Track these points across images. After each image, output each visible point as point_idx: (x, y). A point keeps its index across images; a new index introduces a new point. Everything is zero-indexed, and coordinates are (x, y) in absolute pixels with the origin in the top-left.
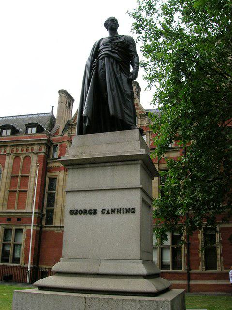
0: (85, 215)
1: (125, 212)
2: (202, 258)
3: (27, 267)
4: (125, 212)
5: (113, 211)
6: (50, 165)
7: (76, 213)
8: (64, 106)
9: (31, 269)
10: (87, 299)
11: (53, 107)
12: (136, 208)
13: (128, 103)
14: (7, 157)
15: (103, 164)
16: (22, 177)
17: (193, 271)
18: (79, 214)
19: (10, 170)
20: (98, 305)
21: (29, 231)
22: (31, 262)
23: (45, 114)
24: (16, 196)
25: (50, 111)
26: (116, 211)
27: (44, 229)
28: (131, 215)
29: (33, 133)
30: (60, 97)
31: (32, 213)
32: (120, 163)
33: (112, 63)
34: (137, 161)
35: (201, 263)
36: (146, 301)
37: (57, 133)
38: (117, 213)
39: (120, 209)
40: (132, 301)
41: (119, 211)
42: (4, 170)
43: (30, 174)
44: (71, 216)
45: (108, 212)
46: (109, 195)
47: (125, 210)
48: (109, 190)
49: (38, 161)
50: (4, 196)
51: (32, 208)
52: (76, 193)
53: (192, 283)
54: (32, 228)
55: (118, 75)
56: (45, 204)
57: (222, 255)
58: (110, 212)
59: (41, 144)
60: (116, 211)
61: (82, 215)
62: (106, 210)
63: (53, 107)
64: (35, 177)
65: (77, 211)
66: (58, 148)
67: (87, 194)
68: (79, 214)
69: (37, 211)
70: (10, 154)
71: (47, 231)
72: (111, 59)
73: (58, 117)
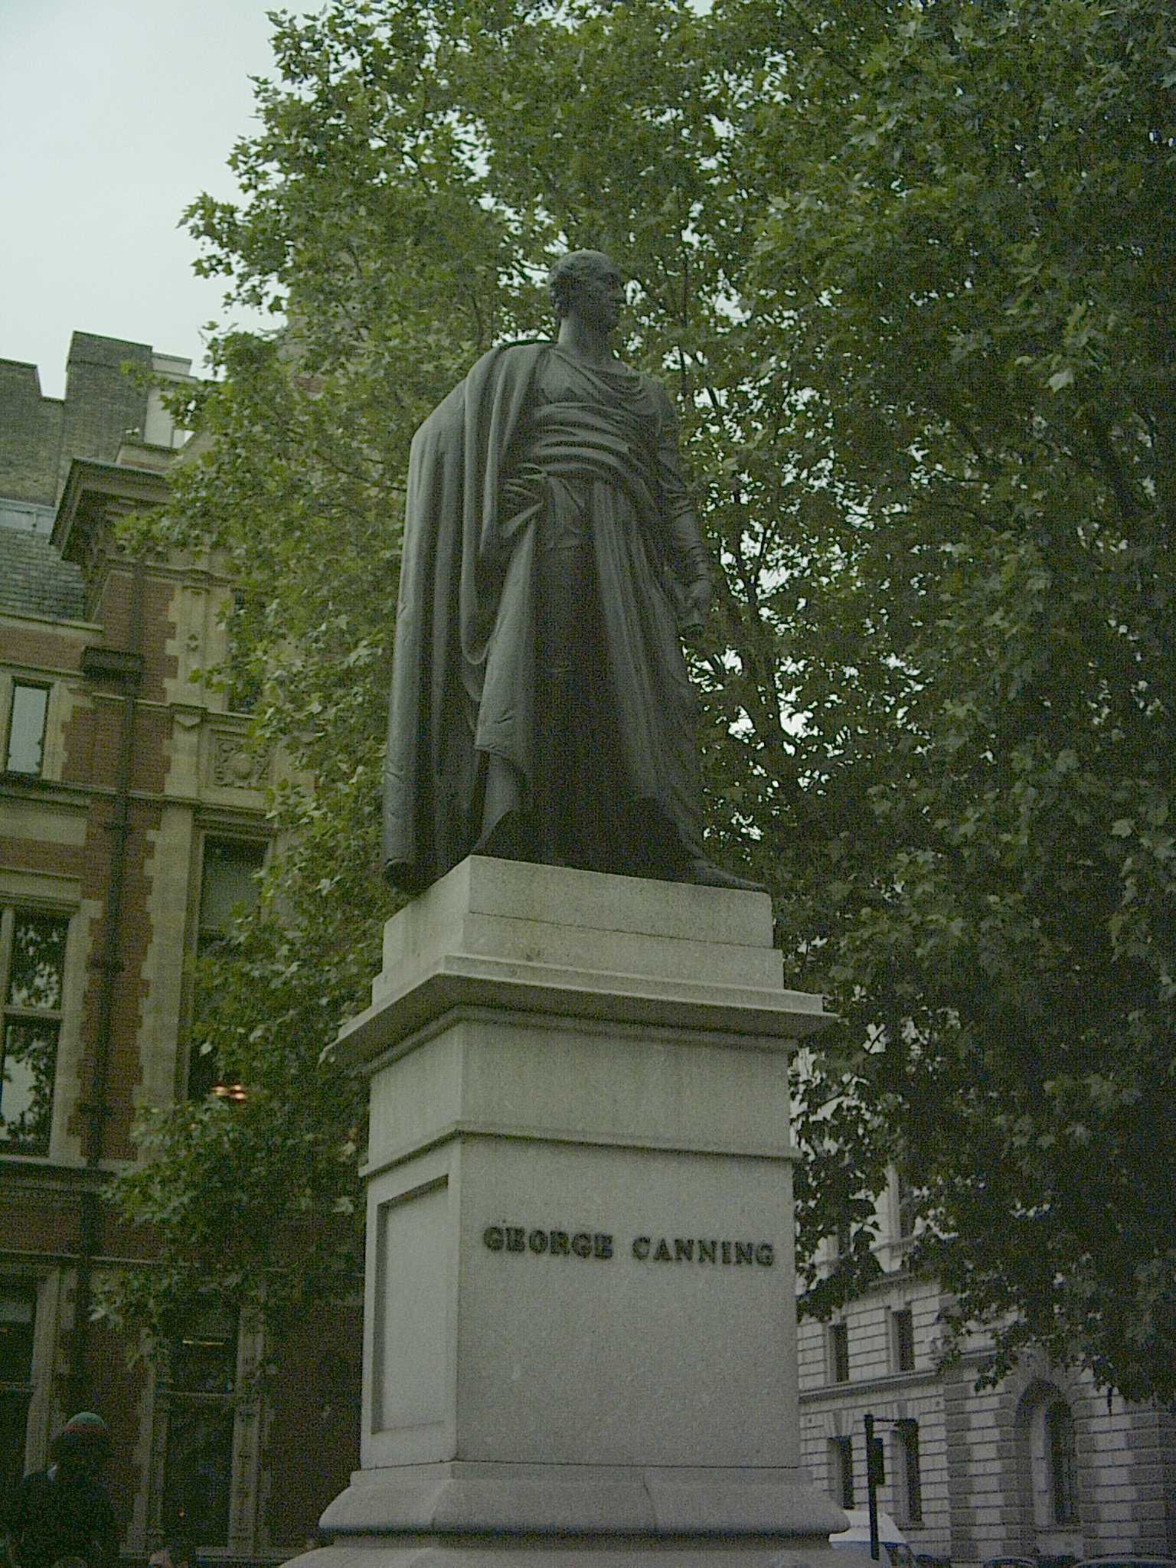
0: (558, 1261)
2: (153, 1472)
5: (684, 1249)
7: (516, 1247)
15: (637, 1030)
26: (622, 1247)
32: (708, 1037)
34: (781, 1042)
38: (701, 1260)
39: (714, 1243)
44: (494, 1258)
45: (662, 1254)
46: (663, 1175)
48: (666, 1151)
52: (509, 1150)
57: (269, 1458)
58: (672, 1252)
60: (696, 1249)
61: (545, 1257)
67: (565, 1159)
68: (528, 1253)
72: (621, 497)
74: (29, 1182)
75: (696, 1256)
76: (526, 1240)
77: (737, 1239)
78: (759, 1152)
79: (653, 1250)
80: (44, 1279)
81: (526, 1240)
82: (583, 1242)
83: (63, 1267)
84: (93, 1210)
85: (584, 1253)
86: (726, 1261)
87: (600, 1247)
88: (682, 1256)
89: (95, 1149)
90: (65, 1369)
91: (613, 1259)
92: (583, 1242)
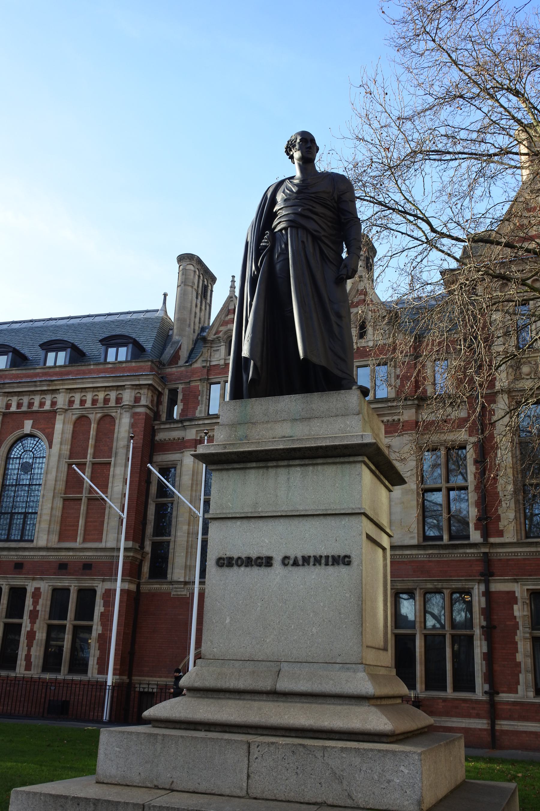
1: (330, 563)
3: (106, 682)
4: (330, 563)
5: (306, 560)
6: (161, 436)
8: (192, 295)
9: (114, 686)
10: (252, 747)
11: (165, 295)
12: (353, 556)
14: (58, 417)
16: (94, 464)
17: (504, 697)
18: (235, 568)
19: (66, 449)
21: (109, 595)
22: (115, 669)
24: (79, 509)
25: (158, 306)
27: (145, 588)
28: (343, 570)
29: (119, 359)
30: (184, 274)
31: (119, 549)
33: (303, 242)
35: (522, 677)
36: (372, 750)
37: (175, 358)
39: (321, 557)
41: (317, 560)
42: (50, 447)
43: (113, 459)
45: (295, 563)
47: (330, 559)
49: (133, 425)
50: (52, 508)
51: (118, 540)
53: (504, 725)
54: (119, 585)
56: (150, 529)
58: (300, 562)
59: (140, 386)
60: (312, 560)
61: (243, 569)
62: (292, 557)
63: (165, 295)
64: (126, 466)
66: (180, 397)
69: (130, 544)
71: (153, 595)
73: (180, 319)
74: (461, 551)
75: (312, 563)
76: (234, 562)
77: (333, 554)
79: (291, 562)
80: (473, 588)
82: (259, 561)
83: (478, 583)
84: (487, 559)
85: (260, 565)
86: (327, 564)
87: (267, 562)
88: (306, 564)
89: (486, 535)
90: (484, 623)
92: (259, 561)
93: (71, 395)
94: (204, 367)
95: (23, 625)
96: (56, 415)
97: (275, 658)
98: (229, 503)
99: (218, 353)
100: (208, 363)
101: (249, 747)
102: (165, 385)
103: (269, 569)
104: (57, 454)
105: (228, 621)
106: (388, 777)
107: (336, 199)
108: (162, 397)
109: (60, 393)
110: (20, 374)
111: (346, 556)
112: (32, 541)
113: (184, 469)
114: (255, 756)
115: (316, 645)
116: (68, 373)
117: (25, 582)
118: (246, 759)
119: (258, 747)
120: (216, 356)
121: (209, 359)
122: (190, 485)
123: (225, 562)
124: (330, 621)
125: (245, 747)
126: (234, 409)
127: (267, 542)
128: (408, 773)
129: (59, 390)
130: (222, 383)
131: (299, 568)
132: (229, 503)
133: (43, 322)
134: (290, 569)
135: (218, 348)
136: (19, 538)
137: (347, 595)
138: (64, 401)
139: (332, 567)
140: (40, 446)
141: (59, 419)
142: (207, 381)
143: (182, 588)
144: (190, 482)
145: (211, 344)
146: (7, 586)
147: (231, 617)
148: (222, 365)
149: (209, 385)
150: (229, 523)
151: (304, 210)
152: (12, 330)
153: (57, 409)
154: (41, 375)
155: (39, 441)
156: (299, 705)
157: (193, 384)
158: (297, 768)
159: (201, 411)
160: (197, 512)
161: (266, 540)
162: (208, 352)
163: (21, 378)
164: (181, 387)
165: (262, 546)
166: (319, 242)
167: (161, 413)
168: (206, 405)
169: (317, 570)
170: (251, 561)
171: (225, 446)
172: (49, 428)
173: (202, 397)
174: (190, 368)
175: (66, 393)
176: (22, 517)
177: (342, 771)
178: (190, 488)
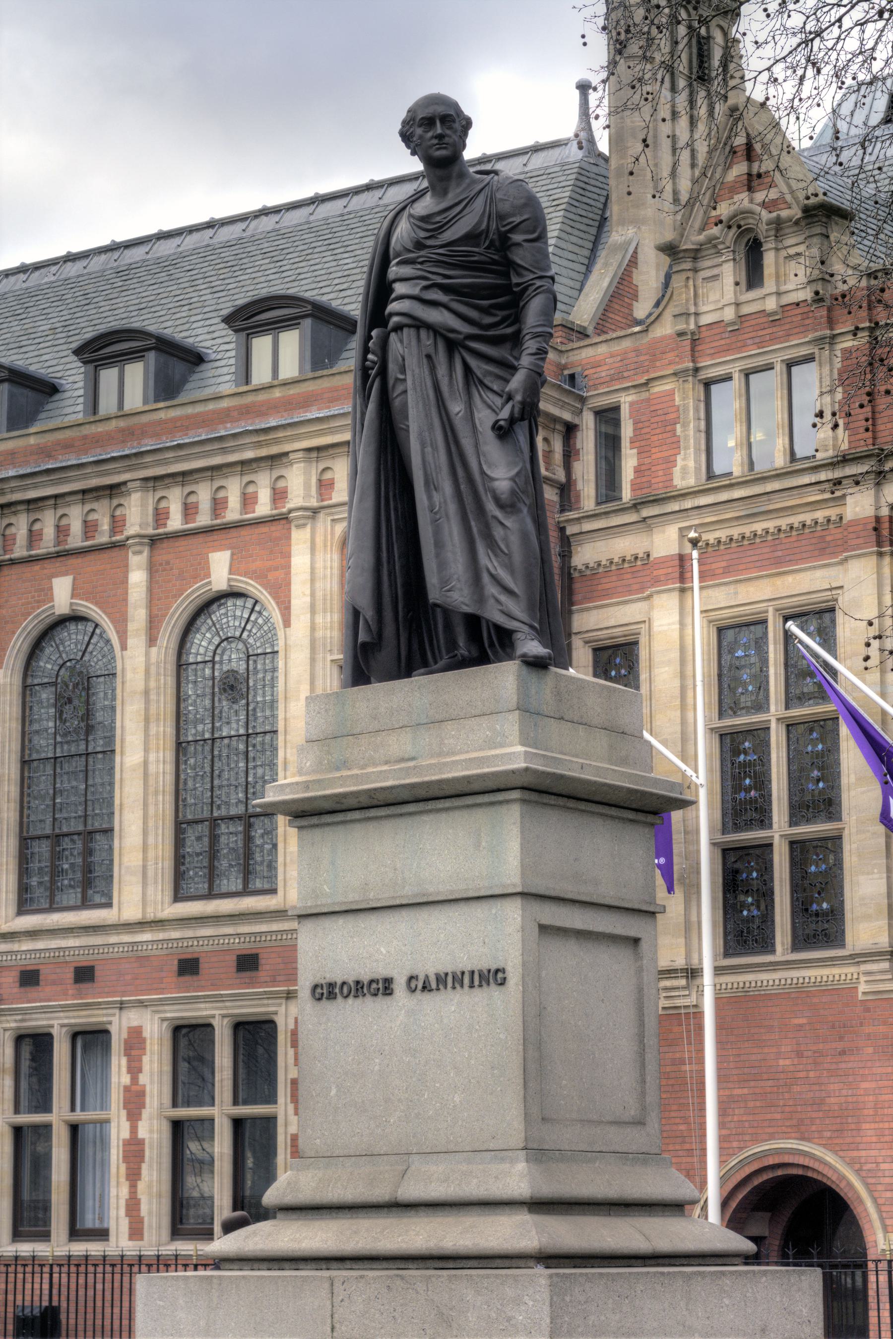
1: (476, 983)
4: (476, 983)
5: (442, 980)
7: (331, 996)
12: (509, 969)
13: (498, 533)
20: (2, 1303)
23: (537, 149)
28: (494, 991)
40: (655, 1273)
45: (426, 988)
55: (456, 408)
58: (434, 986)
60: (450, 980)
61: (350, 1000)
62: (422, 978)
65: (331, 985)
66: (627, 431)
68: (340, 999)
70: (315, 511)
76: (337, 990)
77: (479, 967)
78: (476, 895)
81: (337, 990)
87: (385, 987)
91: (394, 996)
93: (322, 466)
94: (681, 334)
95: (280, 1121)
96: (290, 533)
97: (403, 1150)
98: (325, 887)
99: (717, 284)
100: (692, 319)
101: (332, 1285)
102: (583, 400)
103: (388, 998)
104: (307, 642)
105: (333, 1092)
106: (510, 1314)
107: (497, 244)
108: (579, 434)
109: (291, 464)
110: (180, 418)
111: (319, 999)
112: (273, 891)
113: (657, 646)
114: (340, 1298)
115: (460, 1122)
116: (306, 402)
117: (268, 1005)
118: (328, 1303)
119: (343, 1283)
120: (713, 297)
121: (692, 310)
122: (677, 692)
123: (325, 991)
124: (478, 1082)
125: (327, 1285)
126: (326, 710)
127: (384, 952)
128: (533, 1306)
129: (286, 454)
130: (736, 376)
131: (432, 994)
132: (325, 887)
133: (243, 225)
134: (420, 998)
135: (715, 271)
136: (240, 887)
137: (501, 1036)
138: (307, 486)
139: (480, 989)
140: (260, 621)
141: (300, 539)
142: (695, 376)
143: (684, 988)
144: (677, 683)
145: (695, 259)
146: (226, 1021)
147: (338, 1086)
148: (733, 323)
149: (701, 388)
150: (327, 922)
151: (426, 288)
152: (158, 262)
153: (290, 511)
154: (235, 414)
155: (257, 608)
156: (426, 1220)
157: (658, 388)
158: (395, 1310)
159: (684, 469)
160: (690, 772)
161: (382, 949)
162: (686, 286)
163: (185, 429)
164: (626, 401)
165: (377, 961)
166: (462, 351)
167: (580, 486)
168: (697, 450)
169: (458, 996)
170: (362, 988)
171: (307, 786)
172: (276, 569)
173: (685, 426)
174: (646, 340)
175: (308, 460)
176: (240, 829)
177: (451, 1309)
178: (678, 702)
